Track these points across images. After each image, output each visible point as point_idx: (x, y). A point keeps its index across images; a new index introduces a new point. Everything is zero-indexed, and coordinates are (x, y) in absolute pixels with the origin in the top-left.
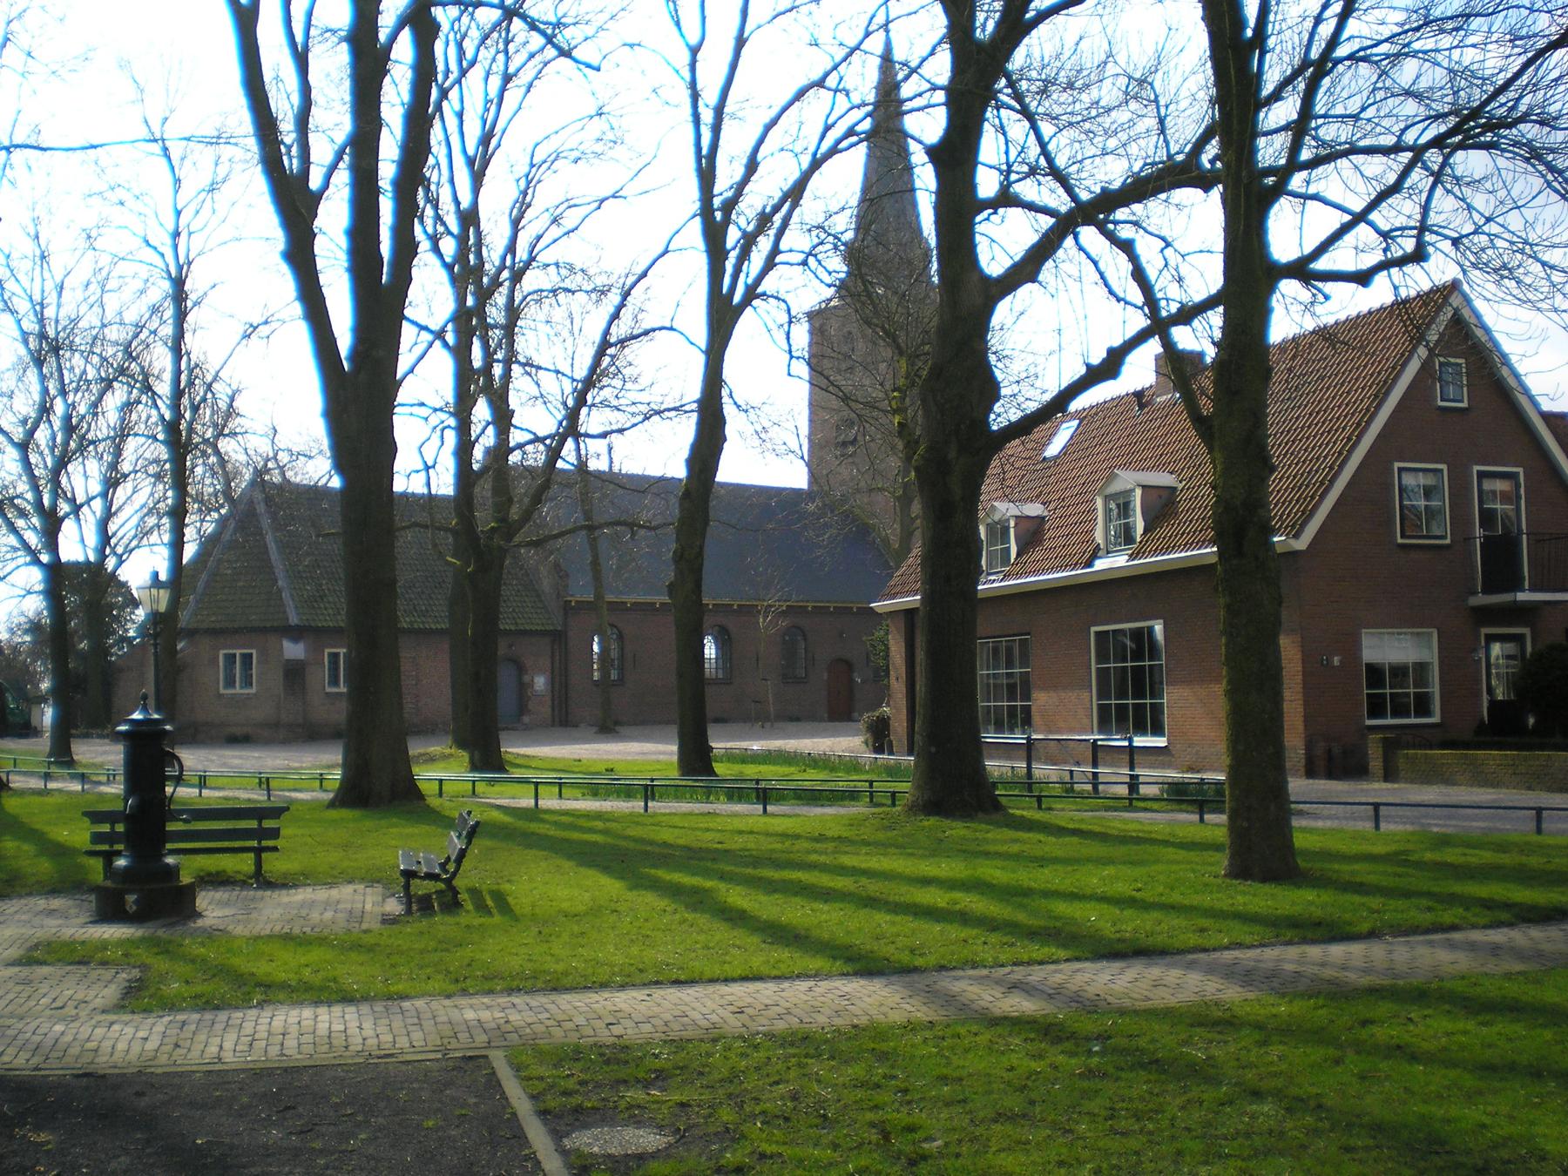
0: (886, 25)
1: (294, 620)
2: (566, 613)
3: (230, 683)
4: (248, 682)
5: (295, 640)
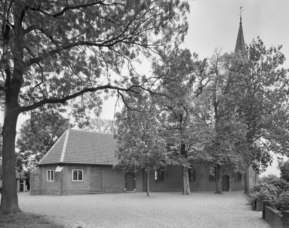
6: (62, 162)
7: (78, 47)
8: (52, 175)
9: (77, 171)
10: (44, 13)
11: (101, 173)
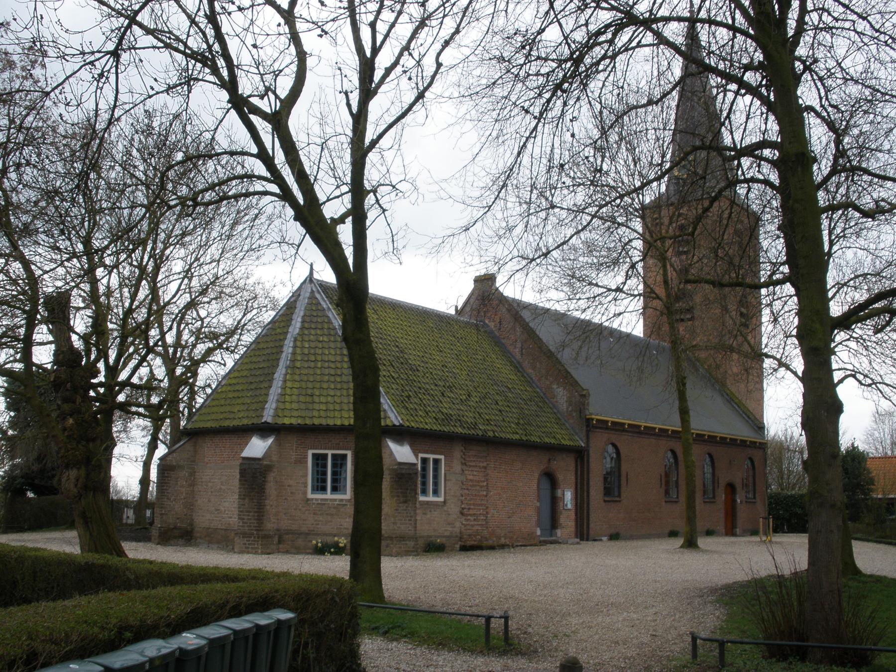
2: (588, 432)
6: (269, 420)
7: (210, 47)
8: (436, 477)
9: (326, 455)
10: (769, 95)
11: (485, 468)
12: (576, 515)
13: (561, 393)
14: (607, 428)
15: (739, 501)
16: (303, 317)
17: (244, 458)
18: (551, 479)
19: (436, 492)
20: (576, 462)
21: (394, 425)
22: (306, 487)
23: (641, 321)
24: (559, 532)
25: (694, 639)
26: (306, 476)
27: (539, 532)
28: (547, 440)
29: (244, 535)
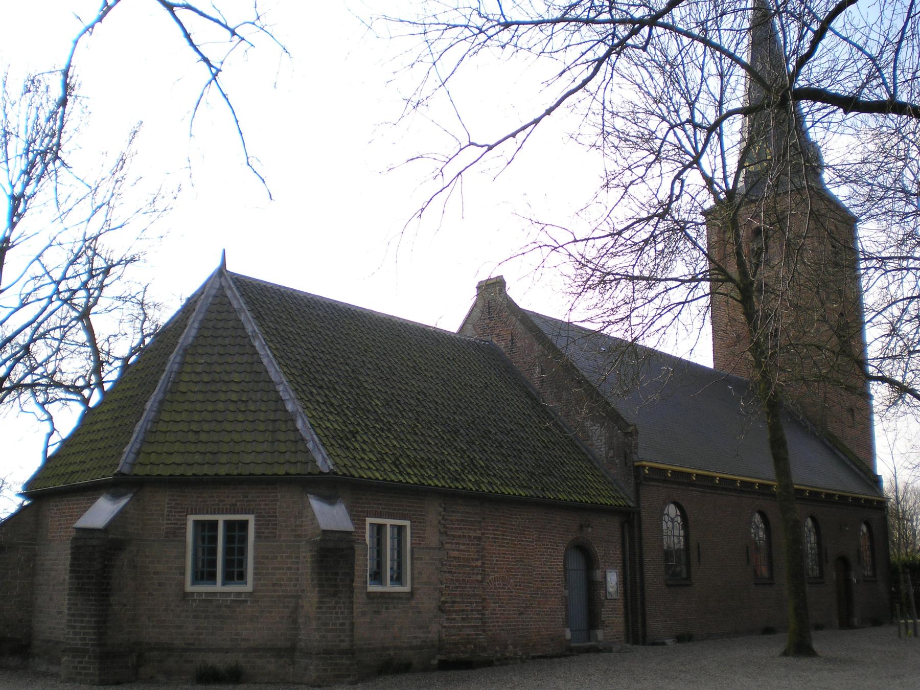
0: (215, 76)
1: (323, 462)
2: (638, 485)
3: (205, 574)
4: (235, 573)
5: (330, 499)
6: (126, 470)
9: (214, 524)
11: (479, 539)
12: (626, 607)
13: (598, 433)
14: (666, 481)
15: (855, 580)
16: (201, 322)
17: (79, 530)
18: (585, 553)
19: (398, 579)
20: (623, 528)
21: (321, 473)
22: (183, 574)
23: (708, 327)
24: (600, 634)
25: (747, 548)
26: (183, 556)
27: (568, 634)
28: (575, 497)
29: (76, 652)
